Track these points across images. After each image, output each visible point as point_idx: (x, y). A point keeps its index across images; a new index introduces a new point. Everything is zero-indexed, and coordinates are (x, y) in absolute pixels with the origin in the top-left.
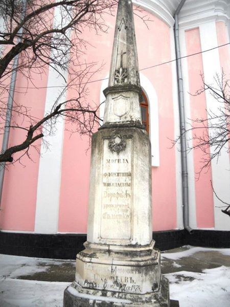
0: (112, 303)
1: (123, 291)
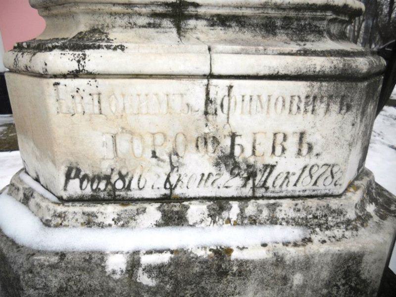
0: (222, 253)
1: (260, 192)
